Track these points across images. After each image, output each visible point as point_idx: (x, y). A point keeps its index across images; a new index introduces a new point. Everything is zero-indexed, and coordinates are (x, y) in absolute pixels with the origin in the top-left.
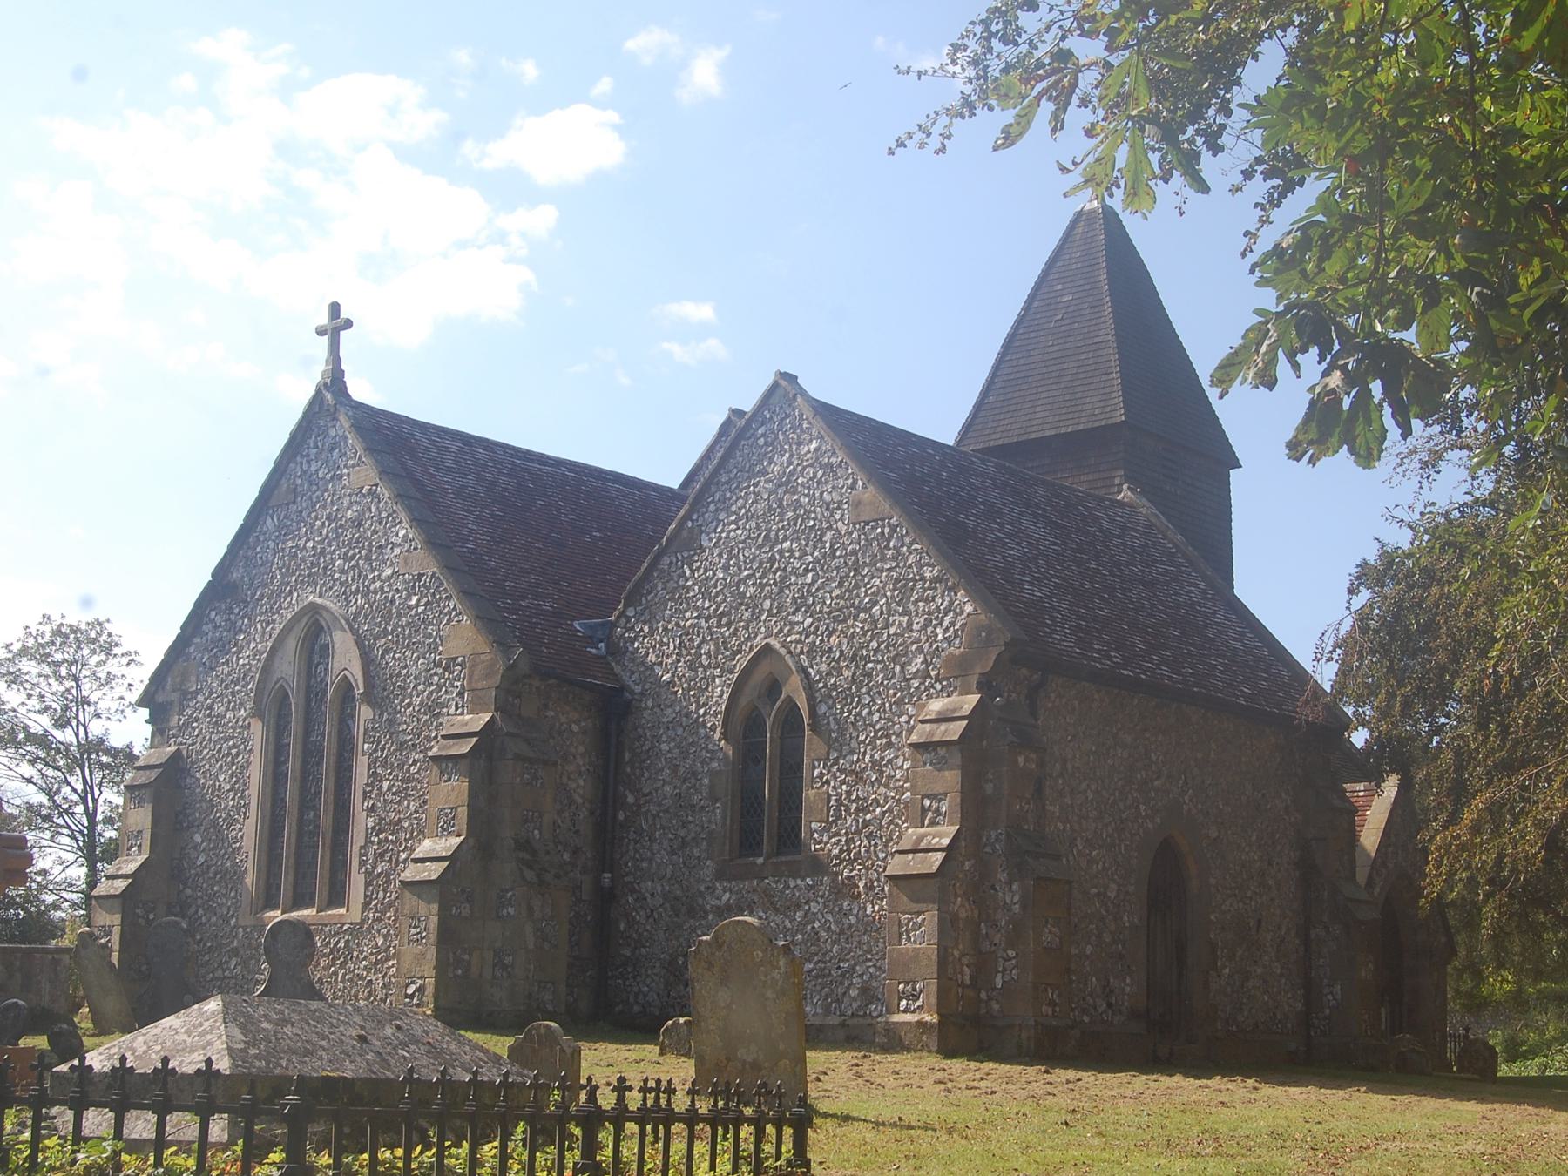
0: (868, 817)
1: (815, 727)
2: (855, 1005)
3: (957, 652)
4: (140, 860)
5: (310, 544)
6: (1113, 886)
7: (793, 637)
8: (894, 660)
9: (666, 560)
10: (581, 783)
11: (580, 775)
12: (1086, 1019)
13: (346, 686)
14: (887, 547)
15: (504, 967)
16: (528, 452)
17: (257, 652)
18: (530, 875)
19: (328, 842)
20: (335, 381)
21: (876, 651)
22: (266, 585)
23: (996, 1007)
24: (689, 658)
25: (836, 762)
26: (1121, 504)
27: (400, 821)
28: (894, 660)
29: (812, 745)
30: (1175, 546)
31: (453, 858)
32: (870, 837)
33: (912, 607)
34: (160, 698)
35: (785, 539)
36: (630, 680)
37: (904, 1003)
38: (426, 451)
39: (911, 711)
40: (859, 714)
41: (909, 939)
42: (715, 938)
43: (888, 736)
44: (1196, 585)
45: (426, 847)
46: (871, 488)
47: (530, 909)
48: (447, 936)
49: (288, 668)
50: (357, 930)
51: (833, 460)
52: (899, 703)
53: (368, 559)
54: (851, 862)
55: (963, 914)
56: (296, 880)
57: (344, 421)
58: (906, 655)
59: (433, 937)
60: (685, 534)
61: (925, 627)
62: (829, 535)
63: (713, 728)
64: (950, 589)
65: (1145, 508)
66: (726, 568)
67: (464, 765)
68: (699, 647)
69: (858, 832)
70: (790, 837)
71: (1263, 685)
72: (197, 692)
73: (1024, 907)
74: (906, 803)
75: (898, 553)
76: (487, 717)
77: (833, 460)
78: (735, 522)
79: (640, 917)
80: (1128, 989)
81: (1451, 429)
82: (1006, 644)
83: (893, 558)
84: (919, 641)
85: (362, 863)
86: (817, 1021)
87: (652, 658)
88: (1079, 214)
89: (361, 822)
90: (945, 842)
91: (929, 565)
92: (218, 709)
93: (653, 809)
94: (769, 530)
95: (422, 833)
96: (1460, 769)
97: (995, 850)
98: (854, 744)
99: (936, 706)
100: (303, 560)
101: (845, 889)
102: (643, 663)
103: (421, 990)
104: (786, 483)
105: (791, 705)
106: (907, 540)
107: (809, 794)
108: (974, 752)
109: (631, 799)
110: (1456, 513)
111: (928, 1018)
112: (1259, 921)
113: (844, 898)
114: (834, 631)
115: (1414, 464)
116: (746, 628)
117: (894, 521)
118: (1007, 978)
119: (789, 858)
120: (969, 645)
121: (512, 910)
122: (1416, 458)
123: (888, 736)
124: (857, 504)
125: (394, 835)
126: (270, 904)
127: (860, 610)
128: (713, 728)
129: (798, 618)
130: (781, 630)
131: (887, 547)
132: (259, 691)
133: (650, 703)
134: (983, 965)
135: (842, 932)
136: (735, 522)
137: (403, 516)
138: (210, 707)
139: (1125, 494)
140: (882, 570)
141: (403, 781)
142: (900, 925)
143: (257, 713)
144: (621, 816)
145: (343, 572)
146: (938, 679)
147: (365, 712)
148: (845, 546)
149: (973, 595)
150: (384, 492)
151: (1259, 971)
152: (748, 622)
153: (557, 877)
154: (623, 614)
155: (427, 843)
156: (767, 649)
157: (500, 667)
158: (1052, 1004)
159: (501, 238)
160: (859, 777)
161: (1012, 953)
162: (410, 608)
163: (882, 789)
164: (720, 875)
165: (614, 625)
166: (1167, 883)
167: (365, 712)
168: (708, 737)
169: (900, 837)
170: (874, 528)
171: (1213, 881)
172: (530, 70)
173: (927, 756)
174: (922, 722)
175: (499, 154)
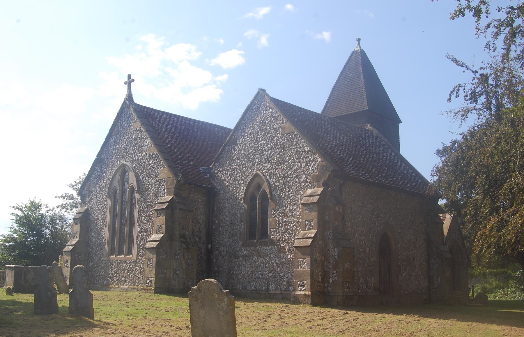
0: (289, 227)
1: (272, 199)
2: (285, 287)
3: (316, 174)
4: (77, 240)
5: (123, 146)
6: (368, 248)
7: (265, 171)
8: (296, 177)
9: (227, 148)
10: (202, 216)
11: (201, 214)
12: (360, 291)
13: (132, 188)
14: (293, 141)
15: (177, 274)
16: (190, 119)
17: (109, 179)
18: (184, 246)
19: (128, 235)
20: (130, 98)
21: (290, 174)
22: (111, 159)
23: (330, 289)
24: (233, 179)
25: (278, 209)
26: (368, 130)
27: (147, 229)
28: (296, 177)
29: (271, 205)
30: (385, 142)
31: (161, 241)
32: (289, 233)
33: (301, 160)
34: (83, 193)
35: (262, 140)
36: (216, 185)
37: (300, 288)
38: (157, 118)
39: (302, 193)
40: (285, 194)
41: (301, 267)
42: (198, 288)
43: (294, 201)
44: (391, 154)
45: (154, 237)
46: (288, 123)
47: (184, 256)
48: (159, 265)
49: (117, 183)
50: (135, 262)
51: (276, 115)
52: (298, 191)
53: (138, 150)
54: (283, 241)
55: (319, 259)
56: (119, 246)
57: (132, 109)
58: (300, 175)
59: (154, 265)
60: (232, 140)
61: (306, 166)
62: (275, 138)
63: (241, 200)
64: (313, 154)
65: (375, 131)
66: (244, 150)
67: (164, 212)
68: (237, 174)
69: (285, 232)
70: (264, 233)
71: (414, 184)
72: (93, 191)
73: (338, 257)
74: (300, 223)
75: (297, 143)
76: (171, 197)
77: (276, 115)
78: (247, 136)
79: (220, 258)
80: (373, 281)
81: (474, 102)
82: (332, 171)
83: (295, 145)
84: (304, 171)
85: (137, 242)
86: (273, 292)
87: (223, 178)
88: (353, 52)
89: (137, 229)
90: (313, 235)
91: (306, 146)
92: (98, 196)
93: (224, 225)
94: (257, 138)
95: (151, 234)
96: (476, 210)
97: (329, 238)
98: (284, 204)
99: (309, 191)
100: (121, 151)
101: (281, 250)
102: (220, 180)
103: (151, 281)
104: (262, 123)
105: (264, 192)
106: (300, 139)
107: (270, 220)
108: (321, 206)
109: (217, 222)
110: (476, 128)
111: (307, 293)
112: (414, 258)
113: (281, 253)
114: (277, 168)
115: (459, 116)
116: (250, 168)
117: (295, 133)
118: (333, 280)
119: (264, 240)
120: (320, 172)
121: (179, 257)
122: (460, 113)
123: (294, 201)
124: (284, 128)
125: (146, 233)
126: (112, 254)
127: (285, 161)
128: (241, 200)
129: (266, 165)
130: (261, 169)
131: (293, 141)
132: (109, 190)
133: (222, 192)
134: (326, 276)
135: (281, 264)
136: (247, 136)
137: (148, 136)
138: (96, 195)
139: (369, 127)
140: (292, 149)
141: (149, 217)
142: (298, 262)
143: (108, 197)
144: (214, 227)
145: (132, 154)
146: (310, 183)
147: (137, 196)
148: (280, 142)
149: (321, 156)
150: (143, 130)
151: (414, 274)
152: (251, 166)
153: (193, 246)
154: (214, 165)
155: (153, 236)
156: (257, 174)
157: (175, 182)
158: (348, 288)
159: (214, 82)
160: (285, 214)
161: (335, 272)
162: (150, 164)
163: (293, 218)
164: (244, 245)
165: (212, 168)
166: (385, 248)
167: (137, 196)
168: (239, 202)
169: (298, 234)
170: (289, 136)
171: (399, 246)
172: (222, 41)
173: (307, 207)
174: (305, 196)
175: (214, 62)
